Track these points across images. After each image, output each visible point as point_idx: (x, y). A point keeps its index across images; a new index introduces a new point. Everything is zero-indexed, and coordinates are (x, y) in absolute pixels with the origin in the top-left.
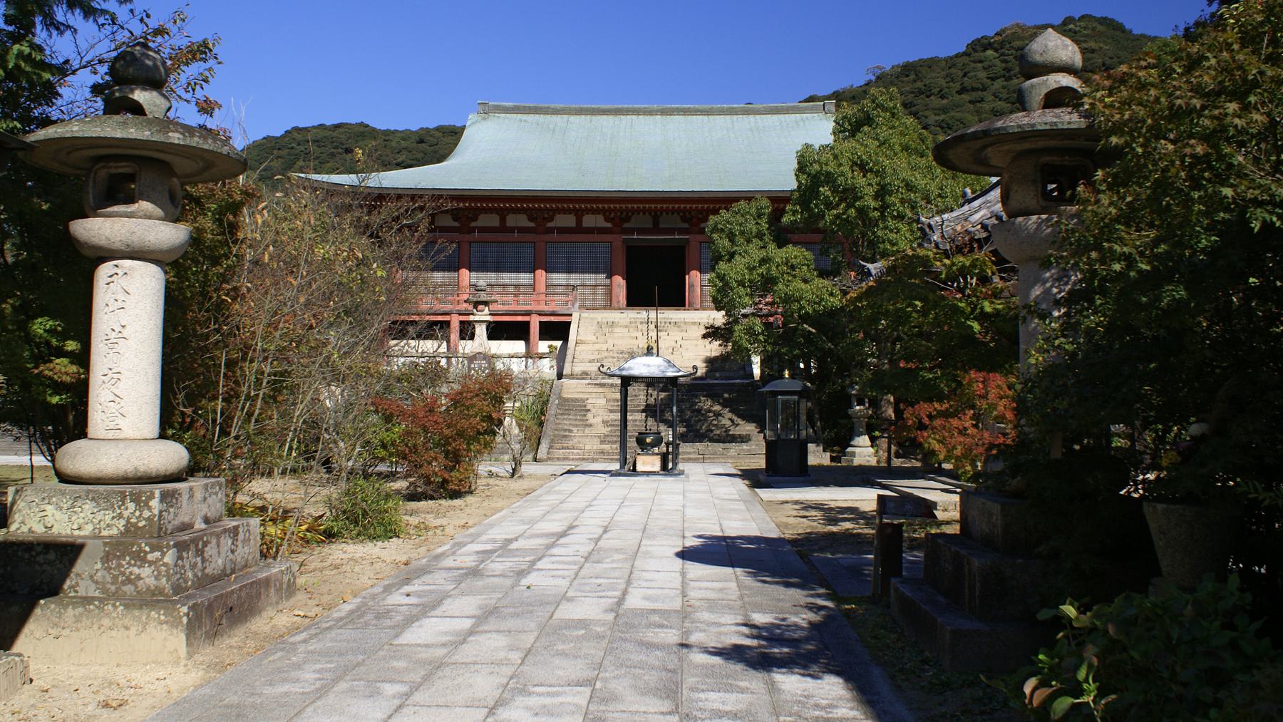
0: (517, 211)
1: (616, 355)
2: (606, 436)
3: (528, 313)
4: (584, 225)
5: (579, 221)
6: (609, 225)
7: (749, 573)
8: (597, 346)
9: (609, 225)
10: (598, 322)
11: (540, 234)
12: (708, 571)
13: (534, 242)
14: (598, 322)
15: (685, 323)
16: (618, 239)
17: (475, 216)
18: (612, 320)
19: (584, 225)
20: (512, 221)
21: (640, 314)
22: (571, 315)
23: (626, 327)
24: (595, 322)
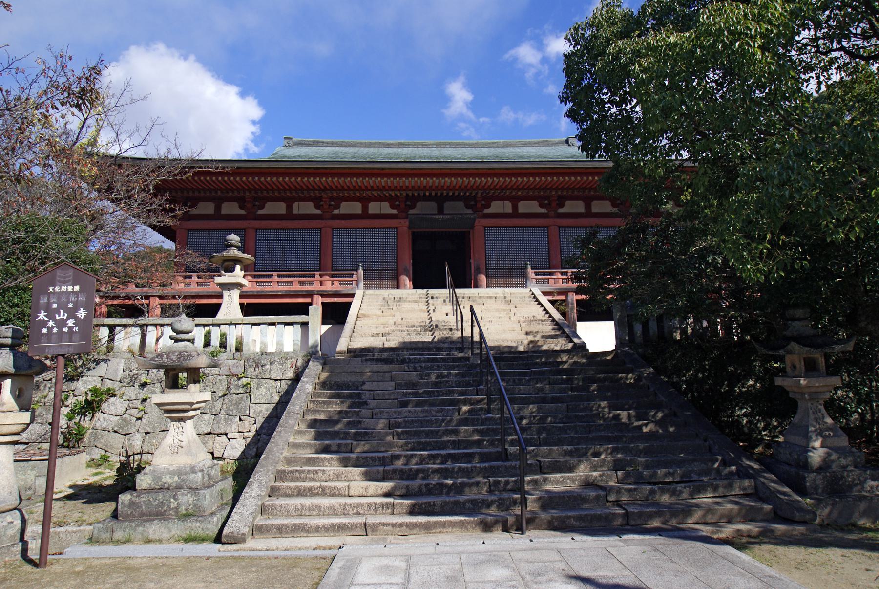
0: (454, 198)
1: (405, 328)
2: (329, 422)
3: (310, 294)
4: (370, 212)
5: (365, 208)
6: (395, 212)
7: (876, 540)
8: (382, 320)
9: (395, 212)
10: (384, 298)
11: (326, 219)
12: (601, 574)
13: (245, 229)
14: (384, 298)
15: (480, 297)
16: (404, 224)
17: (488, 200)
18: (399, 296)
19: (370, 212)
20: (374, 208)
21: (415, 290)
22: (353, 295)
23: (415, 301)
24: (381, 298)
